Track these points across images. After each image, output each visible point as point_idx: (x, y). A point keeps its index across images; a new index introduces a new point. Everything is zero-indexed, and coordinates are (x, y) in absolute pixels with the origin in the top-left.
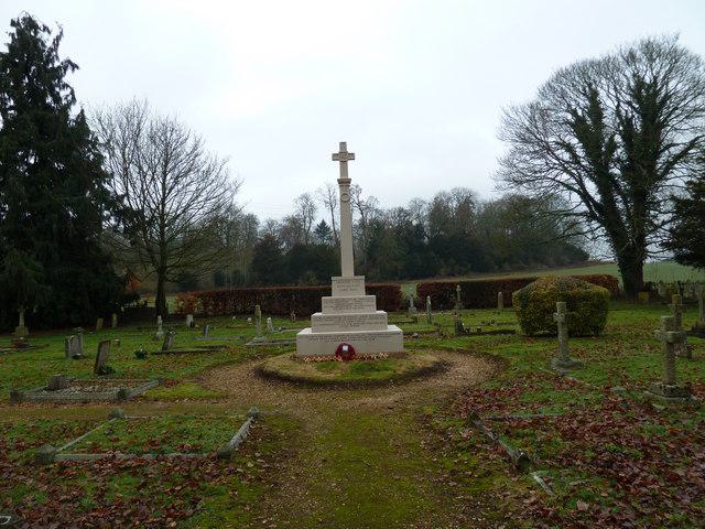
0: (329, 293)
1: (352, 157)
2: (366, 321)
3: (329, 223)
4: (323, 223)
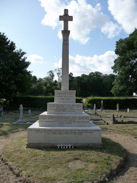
0: (52, 100)
1: (71, 19)
2: (76, 120)
3: (57, 80)
4: (56, 81)
